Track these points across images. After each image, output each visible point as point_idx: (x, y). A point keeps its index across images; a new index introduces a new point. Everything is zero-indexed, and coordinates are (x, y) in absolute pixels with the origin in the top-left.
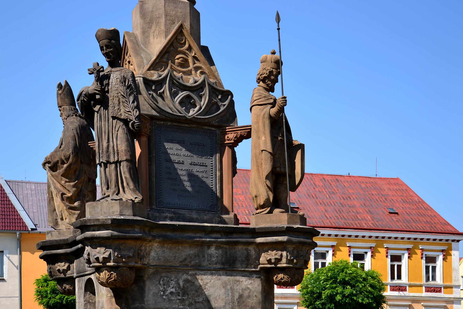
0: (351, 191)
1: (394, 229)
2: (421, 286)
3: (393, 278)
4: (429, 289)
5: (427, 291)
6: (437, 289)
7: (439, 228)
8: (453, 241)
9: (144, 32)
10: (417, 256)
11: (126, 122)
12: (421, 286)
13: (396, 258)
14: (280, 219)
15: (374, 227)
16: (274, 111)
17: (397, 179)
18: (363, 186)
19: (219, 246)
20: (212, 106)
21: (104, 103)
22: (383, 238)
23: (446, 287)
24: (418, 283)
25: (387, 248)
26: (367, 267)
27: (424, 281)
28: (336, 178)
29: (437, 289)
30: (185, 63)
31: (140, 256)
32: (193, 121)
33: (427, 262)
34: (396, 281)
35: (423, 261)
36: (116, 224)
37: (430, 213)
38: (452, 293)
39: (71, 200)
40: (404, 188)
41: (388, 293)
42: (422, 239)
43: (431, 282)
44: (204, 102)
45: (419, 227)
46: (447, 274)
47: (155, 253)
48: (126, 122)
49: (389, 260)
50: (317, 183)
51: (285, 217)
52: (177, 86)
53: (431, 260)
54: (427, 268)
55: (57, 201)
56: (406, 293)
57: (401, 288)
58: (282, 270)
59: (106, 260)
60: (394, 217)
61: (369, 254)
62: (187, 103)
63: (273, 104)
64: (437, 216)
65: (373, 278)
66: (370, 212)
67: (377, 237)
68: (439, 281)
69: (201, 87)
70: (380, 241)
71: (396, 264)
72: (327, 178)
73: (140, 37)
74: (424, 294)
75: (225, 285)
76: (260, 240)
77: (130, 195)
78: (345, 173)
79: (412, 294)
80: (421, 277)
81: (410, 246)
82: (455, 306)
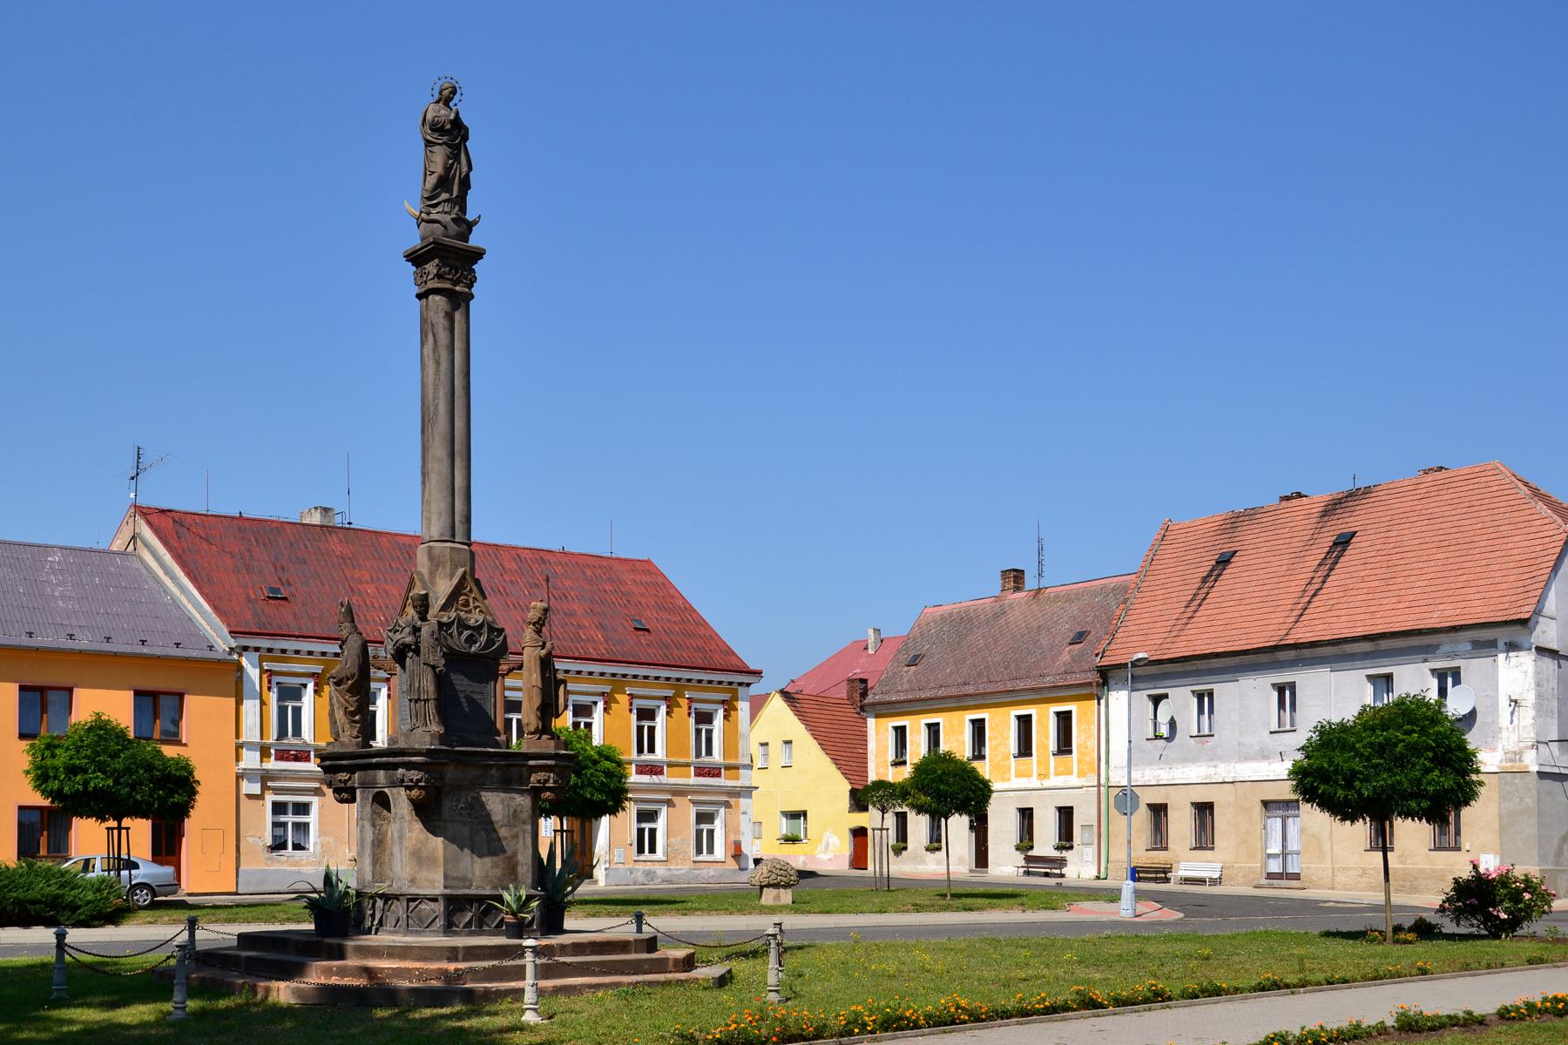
0: (568, 583)
1: (643, 660)
2: (688, 765)
3: (640, 751)
4: (701, 772)
5: (697, 774)
6: (714, 772)
7: (718, 660)
8: (740, 684)
9: (431, 573)
10: (681, 711)
11: (434, 667)
12: (688, 765)
13: (647, 714)
14: (547, 745)
15: (608, 657)
16: (543, 652)
17: (648, 561)
18: (588, 573)
19: (499, 768)
20: (490, 642)
21: (417, 652)
22: (625, 676)
23: (728, 768)
24: (682, 760)
25: (632, 696)
26: (597, 740)
27: (692, 758)
28: (541, 555)
29: (714, 772)
30: (466, 604)
31: (442, 778)
32: (475, 655)
33: (697, 722)
34: (646, 757)
35: (692, 720)
36: (429, 753)
37: (702, 631)
38: (737, 778)
39: (353, 714)
40: (660, 580)
41: (634, 778)
42: (689, 680)
43: (705, 759)
44: (483, 639)
45: (685, 656)
46: (730, 745)
47: (451, 773)
48: (434, 667)
49: (634, 717)
50: (507, 565)
51: (552, 743)
52: (463, 625)
53: (705, 718)
54: (698, 732)
55: (339, 715)
56: (664, 779)
57: (654, 769)
58: (549, 789)
59: (419, 780)
60: (644, 638)
61: (601, 705)
62: (471, 640)
63: (543, 647)
64: (714, 637)
65: (608, 758)
66: (601, 627)
67: (614, 675)
68: (717, 756)
69: (482, 626)
70: (619, 682)
71: (646, 724)
72: (524, 555)
73: (426, 577)
74: (693, 780)
75: (502, 802)
76: (531, 763)
77: (436, 728)
78: (556, 547)
79: (672, 780)
80: (688, 750)
81: (670, 693)
82: (742, 801)
